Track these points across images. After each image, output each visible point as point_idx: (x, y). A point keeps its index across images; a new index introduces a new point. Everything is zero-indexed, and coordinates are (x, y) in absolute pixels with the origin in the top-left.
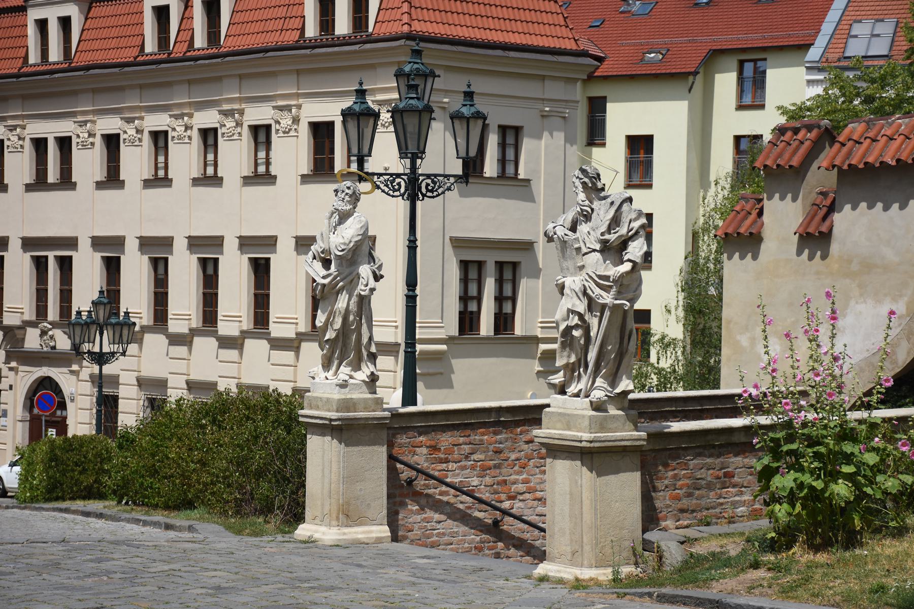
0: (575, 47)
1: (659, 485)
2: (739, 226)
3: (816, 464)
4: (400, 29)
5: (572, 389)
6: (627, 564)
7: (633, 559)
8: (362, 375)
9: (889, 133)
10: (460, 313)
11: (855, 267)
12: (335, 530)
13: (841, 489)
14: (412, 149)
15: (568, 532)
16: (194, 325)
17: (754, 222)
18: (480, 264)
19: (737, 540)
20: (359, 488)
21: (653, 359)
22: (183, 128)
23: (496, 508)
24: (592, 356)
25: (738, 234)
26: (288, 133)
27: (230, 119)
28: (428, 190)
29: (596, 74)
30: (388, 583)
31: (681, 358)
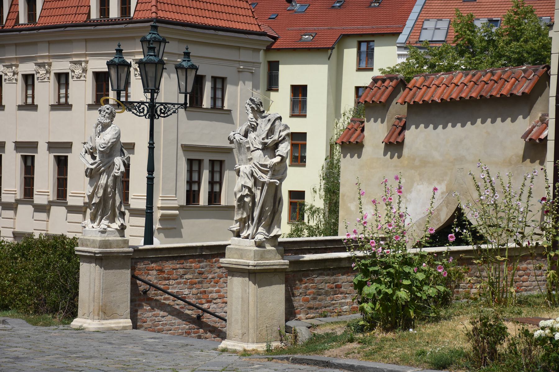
0: (258, 30)
1: (296, 292)
2: (350, 137)
3: (388, 279)
4: (150, 15)
5: (244, 234)
6: (276, 341)
7: (279, 338)
8: (116, 226)
9: (437, 83)
10: (187, 191)
11: (417, 163)
12: (96, 322)
13: (403, 294)
14: (152, 87)
15: (240, 321)
16: (18, 198)
17: (359, 135)
18: (200, 162)
19: (342, 326)
20: (112, 295)
21: (306, 220)
22: (12, 74)
23: (199, 308)
24: (256, 213)
25: (350, 142)
26: (79, 78)
27: (43, 69)
28: (161, 113)
29: (273, 47)
30: (127, 354)
31: (322, 220)
